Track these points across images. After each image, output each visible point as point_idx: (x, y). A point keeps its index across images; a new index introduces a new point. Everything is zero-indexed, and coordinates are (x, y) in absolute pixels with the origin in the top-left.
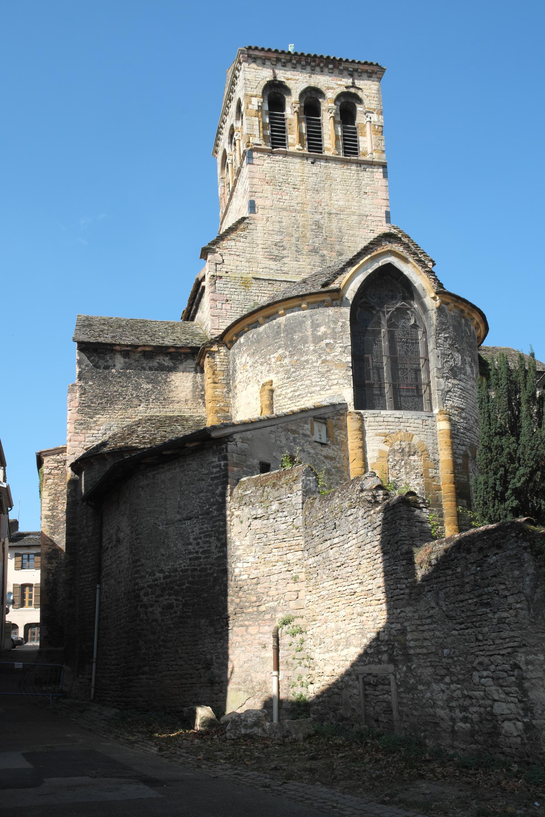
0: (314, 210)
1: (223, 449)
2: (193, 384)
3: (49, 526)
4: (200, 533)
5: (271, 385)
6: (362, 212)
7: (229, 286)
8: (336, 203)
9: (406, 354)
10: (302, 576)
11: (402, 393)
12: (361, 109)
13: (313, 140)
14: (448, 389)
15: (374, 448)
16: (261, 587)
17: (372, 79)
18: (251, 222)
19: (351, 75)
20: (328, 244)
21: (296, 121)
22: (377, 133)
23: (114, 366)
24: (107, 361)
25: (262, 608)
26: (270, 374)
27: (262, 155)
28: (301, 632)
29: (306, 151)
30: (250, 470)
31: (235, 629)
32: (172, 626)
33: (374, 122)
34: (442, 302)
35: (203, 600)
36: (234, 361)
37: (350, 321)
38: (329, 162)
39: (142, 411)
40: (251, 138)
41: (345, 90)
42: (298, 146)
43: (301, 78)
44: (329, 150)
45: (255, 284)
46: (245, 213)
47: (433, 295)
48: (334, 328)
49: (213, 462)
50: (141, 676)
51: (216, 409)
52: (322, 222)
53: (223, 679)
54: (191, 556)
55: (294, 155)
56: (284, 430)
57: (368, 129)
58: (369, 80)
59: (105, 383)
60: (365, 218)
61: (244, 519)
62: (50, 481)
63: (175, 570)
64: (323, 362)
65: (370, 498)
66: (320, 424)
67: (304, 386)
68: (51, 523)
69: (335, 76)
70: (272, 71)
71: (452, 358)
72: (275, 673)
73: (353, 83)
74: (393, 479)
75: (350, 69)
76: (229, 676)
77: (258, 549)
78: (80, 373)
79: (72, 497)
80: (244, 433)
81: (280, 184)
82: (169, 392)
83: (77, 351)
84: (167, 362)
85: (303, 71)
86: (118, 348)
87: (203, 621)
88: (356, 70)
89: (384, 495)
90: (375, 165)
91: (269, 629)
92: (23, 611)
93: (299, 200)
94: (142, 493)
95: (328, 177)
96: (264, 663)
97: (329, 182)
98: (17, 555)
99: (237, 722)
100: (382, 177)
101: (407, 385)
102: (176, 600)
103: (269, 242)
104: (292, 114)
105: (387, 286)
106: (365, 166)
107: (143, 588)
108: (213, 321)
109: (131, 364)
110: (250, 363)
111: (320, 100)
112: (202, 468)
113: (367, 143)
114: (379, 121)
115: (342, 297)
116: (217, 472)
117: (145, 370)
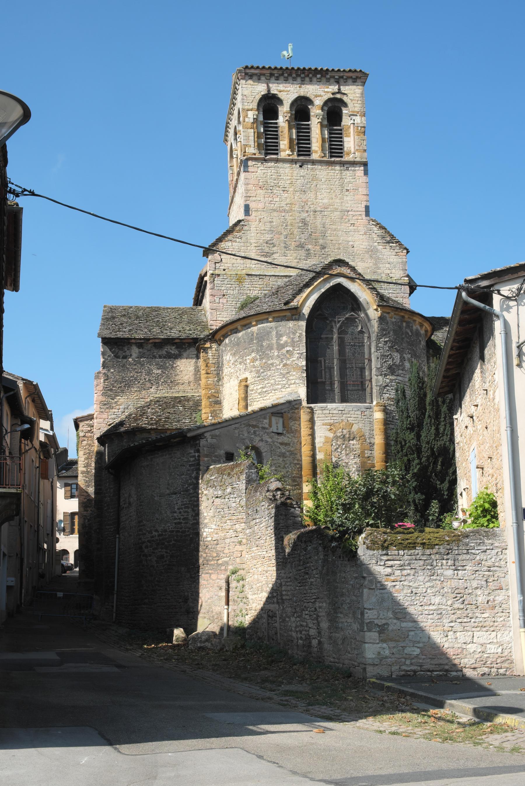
0: (300, 209)
1: (197, 444)
2: (195, 369)
3: (84, 480)
4: (182, 505)
5: (246, 382)
6: (344, 208)
7: (226, 282)
8: (321, 201)
9: (353, 355)
10: (244, 541)
11: (349, 388)
12: (347, 112)
13: (302, 146)
14: (386, 384)
15: (321, 435)
16: (219, 547)
17: (357, 84)
18: (246, 223)
19: (338, 82)
20: (313, 239)
21: (287, 129)
22: (360, 134)
23: (131, 355)
24: (125, 352)
25: (220, 562)
26: (246, 372)
27: (256, 163)
28: (243, 580)
29: (295, 157)
30: (218, 459)
31: (203, 575)
32: (163, 571)
33: (357, 124)
34: (383, 312)
35: (182, 554)
36: (222, 357)
37: (307, 332)
38: (315, 165)
39: (154, 393)
40: (247, 149)
41: (332, 96)
42: (288, 152)
43: (292, 89)
44: (316, 152)
45: (248, 280)
46: (241, 216)
47: (375, 307)
48: (293, 338)
49: (190, 453)
50: (143, 606)
51: (208, 395)
52: (308, 219)
53: (195, 610)
54: (176, 521)
55: (284, 161)
56: (247, 426)
57: (352, 130)
58: (353, 85)
59: (124, 370)
60: (346, 213)
61: (210, 497)
62: (85, 443)
63: (165, 531)
64: (284, 366)
65: (271, 497)
66: (277, 418)
67: (270, 385)
68: (86, 478)
69: (323, 84)
70: (266, 85)
71: (390, 358)
72: (226, 607)
73: (339, 89)
74: (335, 459)
75: (336, 77)
76: (199, 608)
77: (218, 520)
78: (104, 362)
79: (99, 463)
80: (213, 432)
81: (271, 188)
82: (175, 376)
83: (101, 344)
84: (173, 350)
85: (294, 82)
86: (133, 341)
87: (183, 568)
88: (342, 77)
89: (281, 495)
90: (356, 164)
91: (223, 576)
92: (73, 537)
93: (288, 201)
94: (144, 471)
95: (315, 178)
96: (220, 600)
97: (315, 183)
98: (66, 485)
99: (196, 638)
100: (363, 175)
101: (353, 381)
102: (166, 552)
103: (261, 241)
104: (284, 122)
105: (337, 303)
106: (348, 166)
107: (144, 542)
108: (211, 313)
109: (144, 353)
110: (232, 361)
111: (310, 107)
112: (183, 457)
113: (350, 143)
114: (362, 123)
115: (300, 313)
116: (194, 461)
117: (155, 358)
